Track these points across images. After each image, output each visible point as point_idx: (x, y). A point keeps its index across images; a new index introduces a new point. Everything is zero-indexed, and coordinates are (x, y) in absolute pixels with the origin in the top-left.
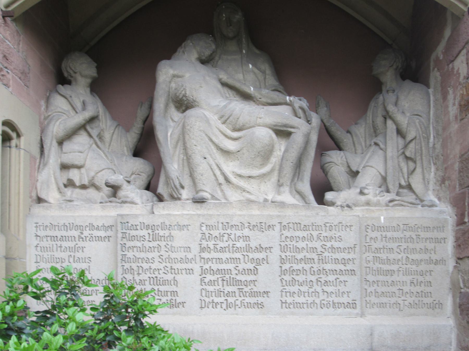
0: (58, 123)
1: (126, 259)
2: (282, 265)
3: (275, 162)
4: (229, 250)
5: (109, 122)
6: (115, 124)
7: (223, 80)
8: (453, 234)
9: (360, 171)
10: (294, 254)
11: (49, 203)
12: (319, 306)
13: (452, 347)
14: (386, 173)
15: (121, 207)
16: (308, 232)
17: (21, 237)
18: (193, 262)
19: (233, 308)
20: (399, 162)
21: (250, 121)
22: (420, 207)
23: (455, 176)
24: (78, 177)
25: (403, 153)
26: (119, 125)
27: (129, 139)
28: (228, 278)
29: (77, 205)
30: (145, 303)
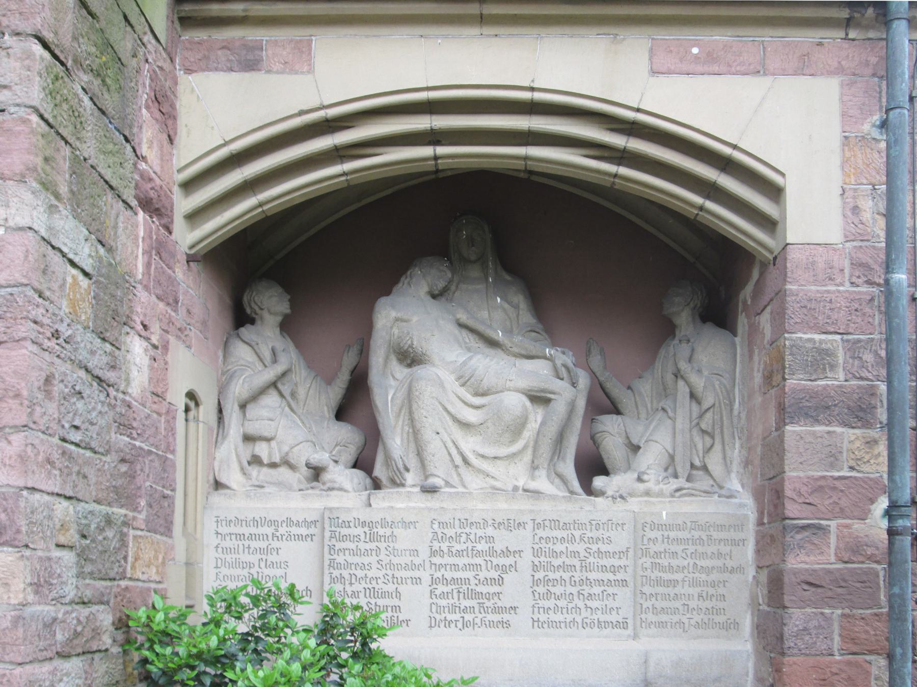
0: (241, 381)
1: (335, 565)
2: (534, 574)
3: (529, 437)
4: (467, 554)
5: (304, 373)
6: (313, 374)
7: (461, 320)
8: (754, 534)
9: (642, 445)
10: (549, 560)
11: (233, 490)
12: (580, 626)
13: (749, 679)
14: (674, 451)
15: (328, 496)
16: (569, 532)
17: (198, 536)
18: (421, 569)
19: (471, 628)
20: (691, 436)
21: (497, 385)
22: (716, 497)
23: (757, 462)
24: (267, 453)
25: (698, 424)
26: (316, 375)
27: (331, 396)
28: (466, 590)
29: (270, 493)
30: (376, 626)
